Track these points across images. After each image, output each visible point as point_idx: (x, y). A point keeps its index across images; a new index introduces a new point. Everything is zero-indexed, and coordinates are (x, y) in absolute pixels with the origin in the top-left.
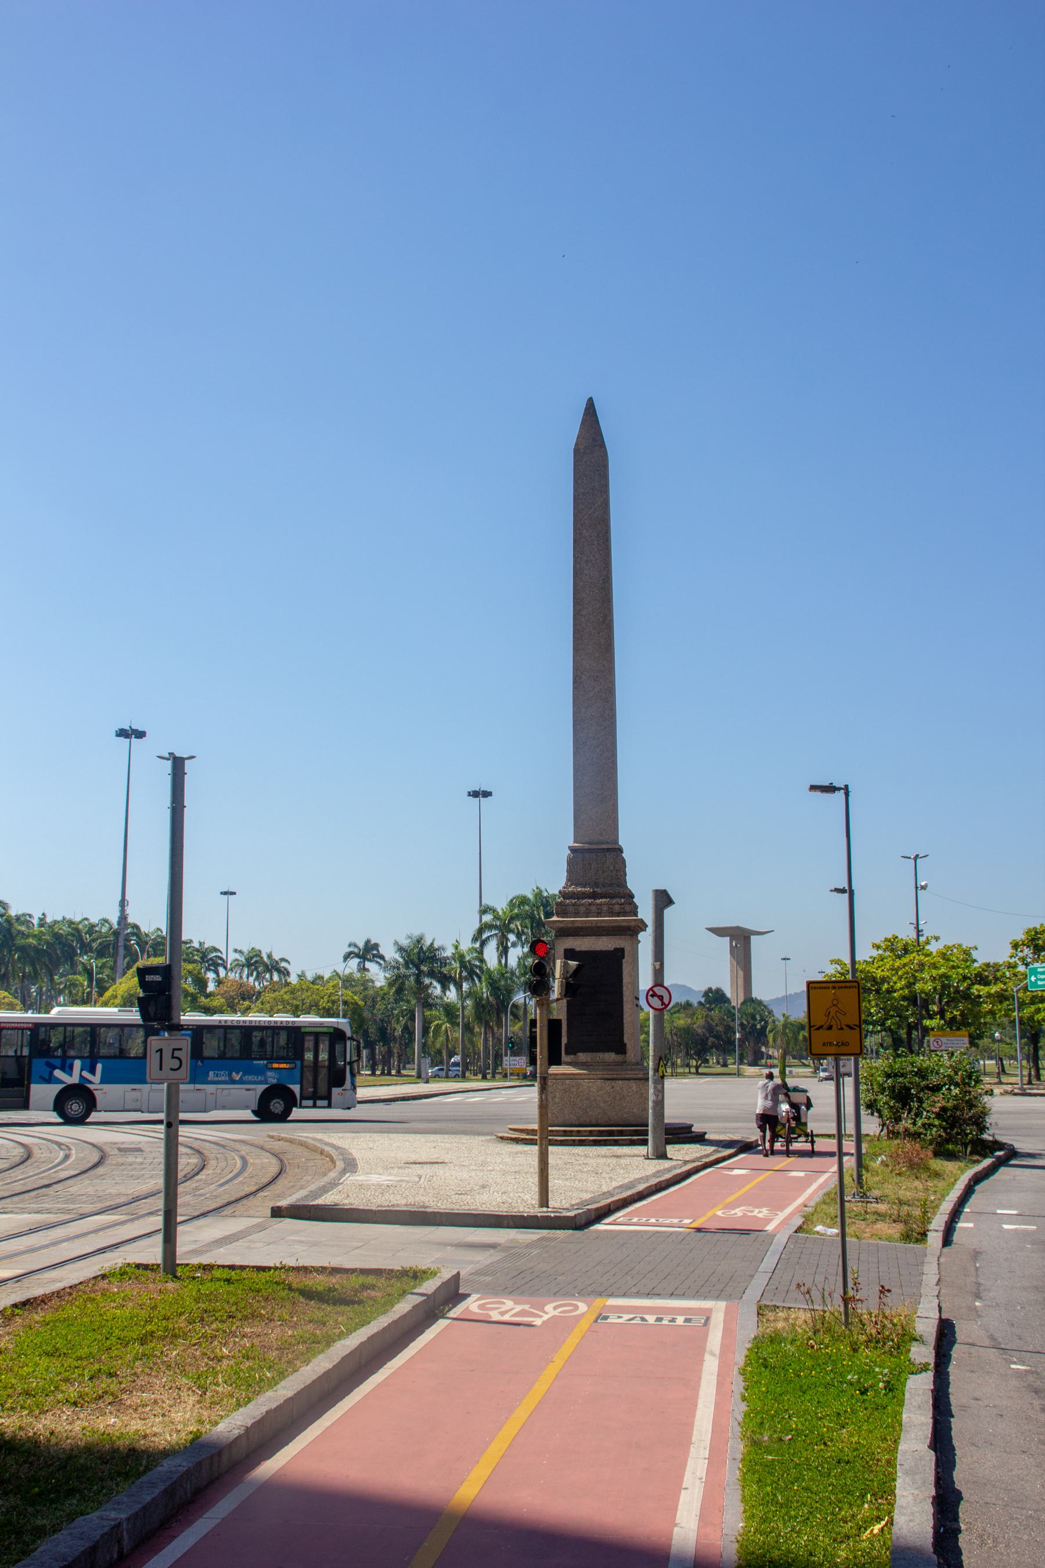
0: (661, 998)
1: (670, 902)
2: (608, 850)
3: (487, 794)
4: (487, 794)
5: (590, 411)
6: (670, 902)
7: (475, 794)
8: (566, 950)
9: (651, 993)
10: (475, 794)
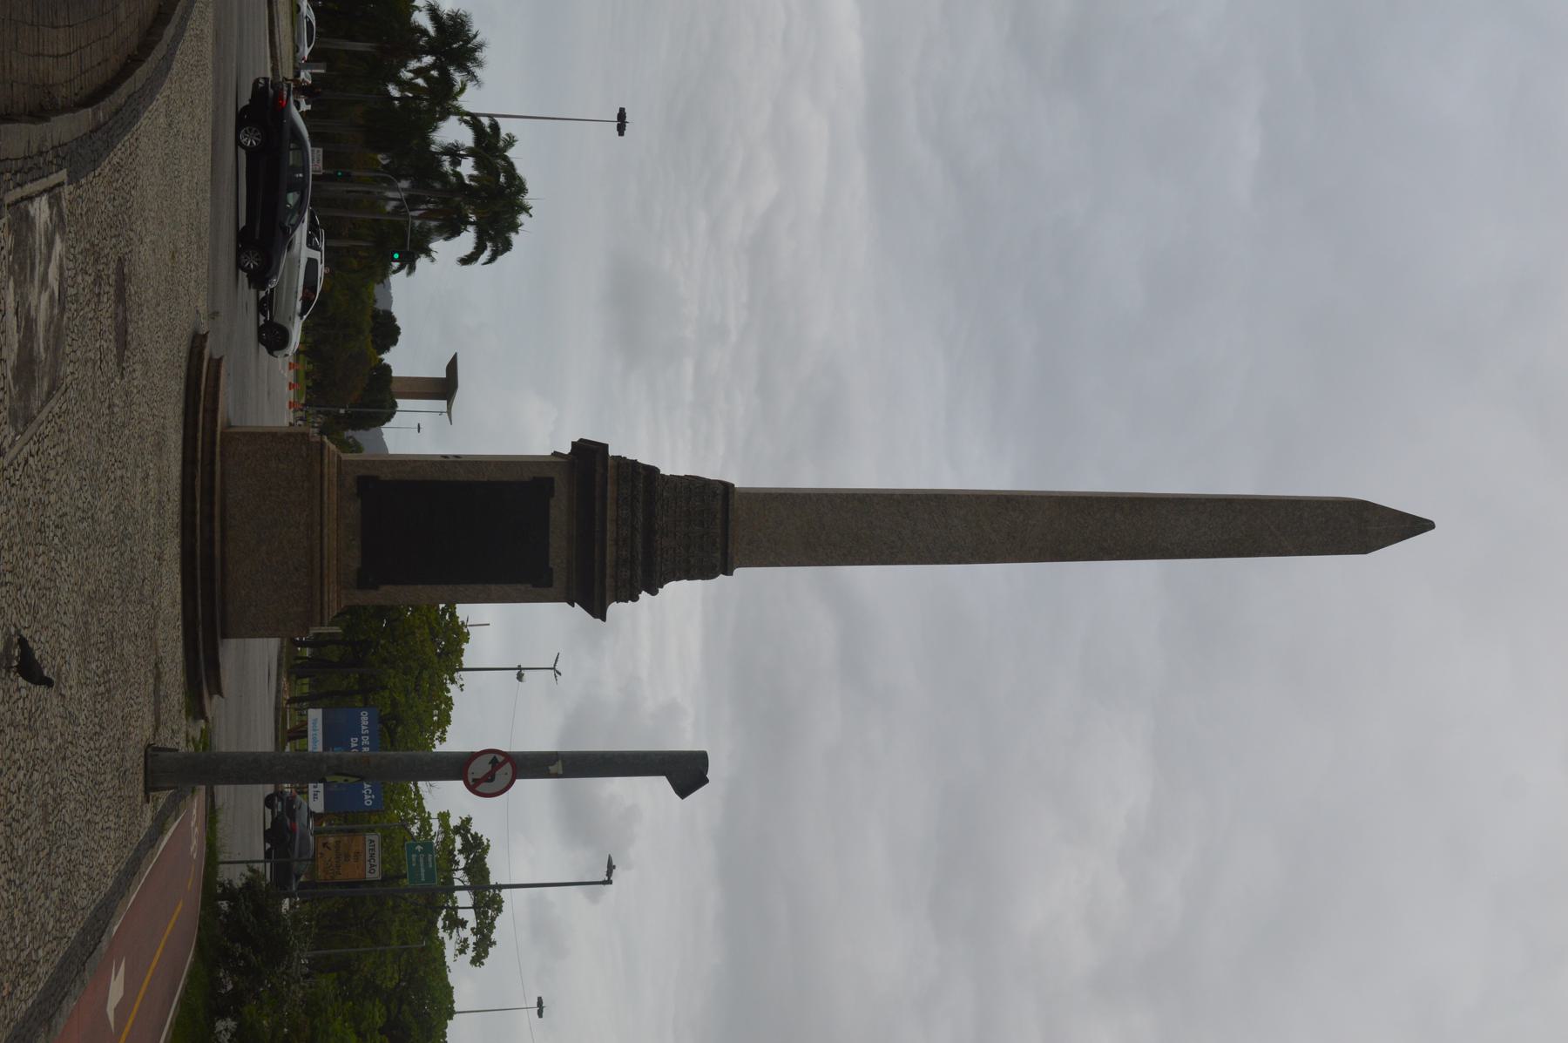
0: (490, 777)
1: (683, 790)
2: (725, 554)
3: (621, 129)
4: (621, 129)
5: (1416, 526)
6: (683, 790)
7: (622, 115)
8: (551, 480)
9: (500, 759)
10: (622, 115)
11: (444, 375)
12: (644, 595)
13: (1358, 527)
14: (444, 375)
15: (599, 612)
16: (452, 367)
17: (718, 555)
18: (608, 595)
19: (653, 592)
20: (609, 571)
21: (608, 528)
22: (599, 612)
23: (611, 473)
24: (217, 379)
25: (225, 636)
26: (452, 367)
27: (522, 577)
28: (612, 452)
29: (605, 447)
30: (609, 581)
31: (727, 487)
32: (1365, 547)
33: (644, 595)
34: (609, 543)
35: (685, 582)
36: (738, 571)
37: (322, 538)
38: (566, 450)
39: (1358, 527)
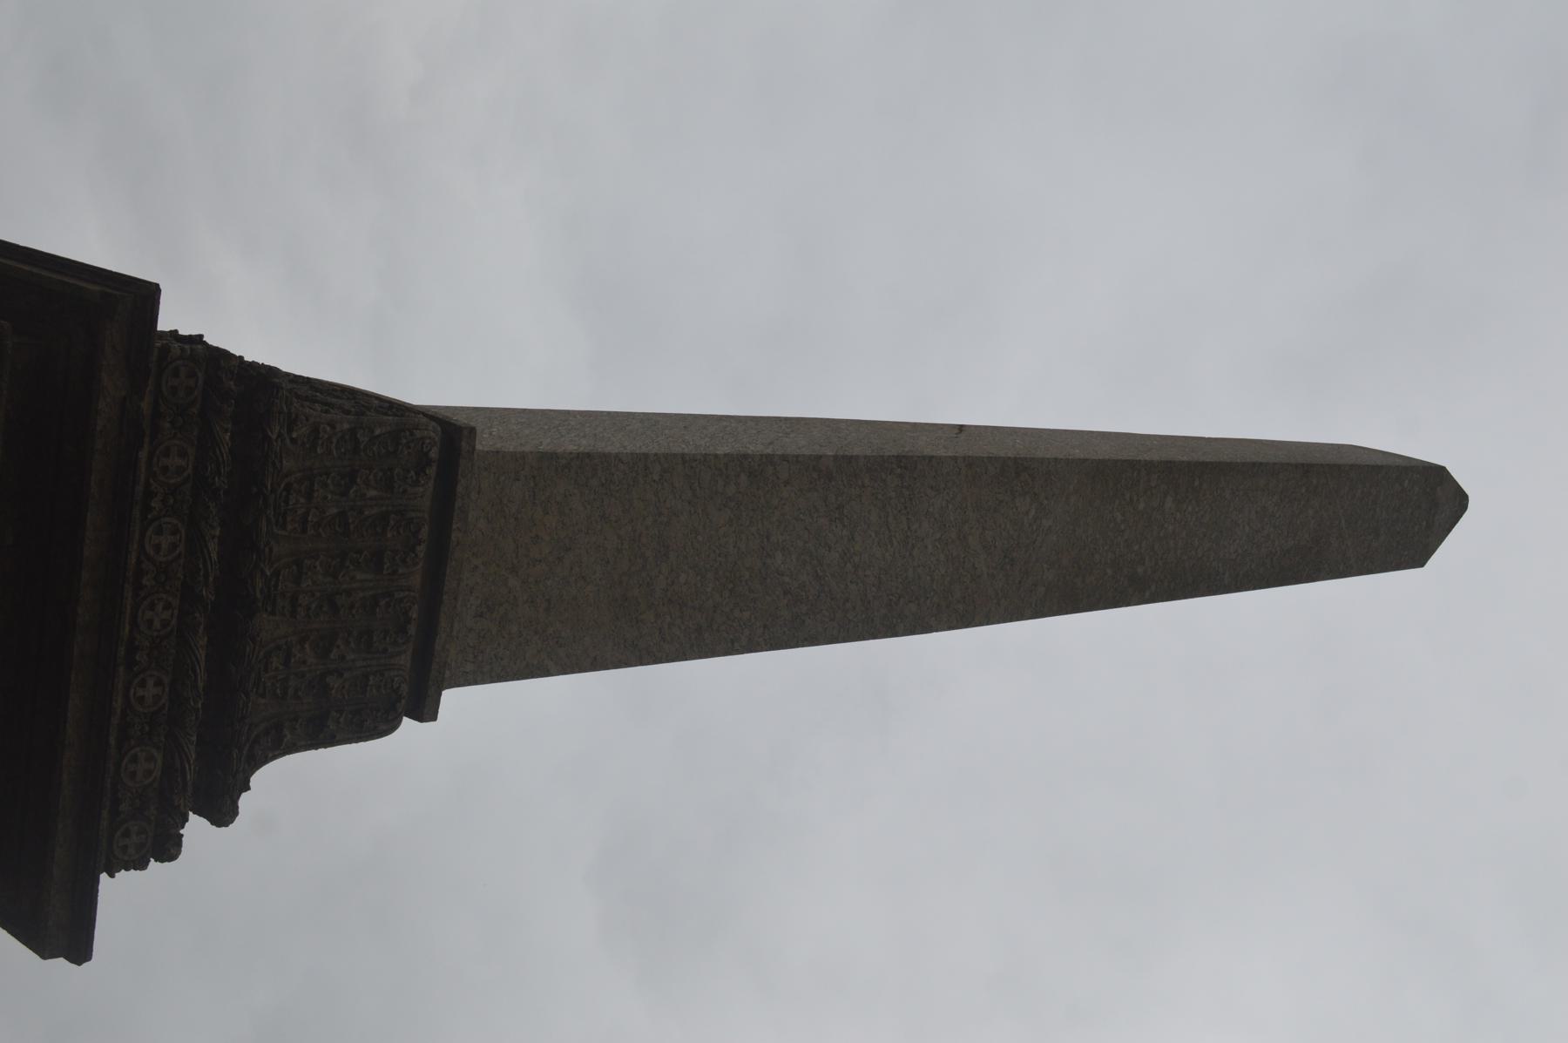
17: (405, 660)
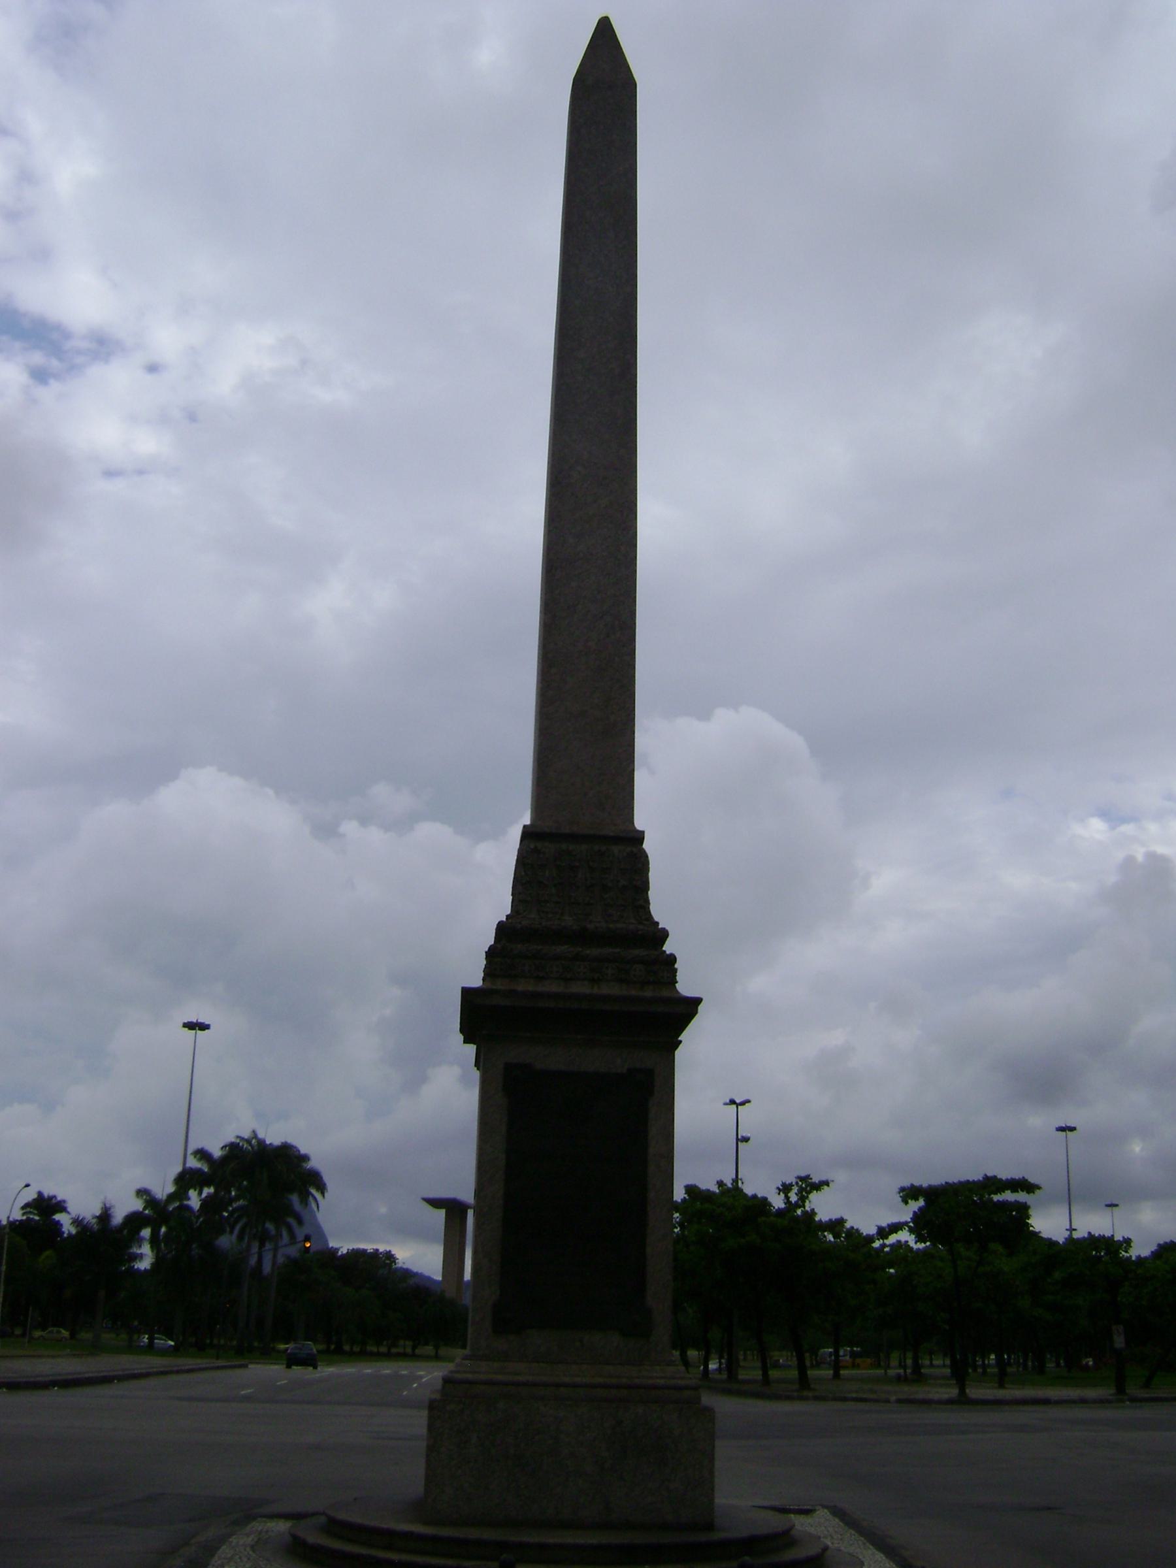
11: (443, 1212)
12: (668, 947)
13: (603, 95)
14: (443, 1212)
15: (692, 1005)
16: (435, 1203)
17: (616, 849)
18: (665, 993)
19: (664, 935)
20: (633, 992)
21: (578, 982)
22: (692, 1005)
23: (500, 985)
24: (361, 1528)
25: (710, 1527)
26: (435, 1203)
27: (646, 1096)
28: (476, 980)
29: (468, 994)
30: (648, 993)
31: (528, 834)
32: (630, 85)
33: (668, 947)
34: (596, 991)
35: (651, 894)
36: (639, 823)
37: (575, 1386)
38: (471, 1049)
39: (603, 95)
